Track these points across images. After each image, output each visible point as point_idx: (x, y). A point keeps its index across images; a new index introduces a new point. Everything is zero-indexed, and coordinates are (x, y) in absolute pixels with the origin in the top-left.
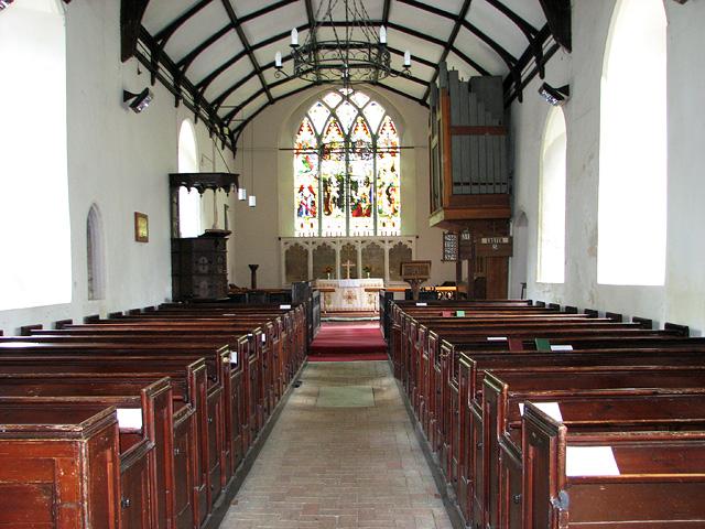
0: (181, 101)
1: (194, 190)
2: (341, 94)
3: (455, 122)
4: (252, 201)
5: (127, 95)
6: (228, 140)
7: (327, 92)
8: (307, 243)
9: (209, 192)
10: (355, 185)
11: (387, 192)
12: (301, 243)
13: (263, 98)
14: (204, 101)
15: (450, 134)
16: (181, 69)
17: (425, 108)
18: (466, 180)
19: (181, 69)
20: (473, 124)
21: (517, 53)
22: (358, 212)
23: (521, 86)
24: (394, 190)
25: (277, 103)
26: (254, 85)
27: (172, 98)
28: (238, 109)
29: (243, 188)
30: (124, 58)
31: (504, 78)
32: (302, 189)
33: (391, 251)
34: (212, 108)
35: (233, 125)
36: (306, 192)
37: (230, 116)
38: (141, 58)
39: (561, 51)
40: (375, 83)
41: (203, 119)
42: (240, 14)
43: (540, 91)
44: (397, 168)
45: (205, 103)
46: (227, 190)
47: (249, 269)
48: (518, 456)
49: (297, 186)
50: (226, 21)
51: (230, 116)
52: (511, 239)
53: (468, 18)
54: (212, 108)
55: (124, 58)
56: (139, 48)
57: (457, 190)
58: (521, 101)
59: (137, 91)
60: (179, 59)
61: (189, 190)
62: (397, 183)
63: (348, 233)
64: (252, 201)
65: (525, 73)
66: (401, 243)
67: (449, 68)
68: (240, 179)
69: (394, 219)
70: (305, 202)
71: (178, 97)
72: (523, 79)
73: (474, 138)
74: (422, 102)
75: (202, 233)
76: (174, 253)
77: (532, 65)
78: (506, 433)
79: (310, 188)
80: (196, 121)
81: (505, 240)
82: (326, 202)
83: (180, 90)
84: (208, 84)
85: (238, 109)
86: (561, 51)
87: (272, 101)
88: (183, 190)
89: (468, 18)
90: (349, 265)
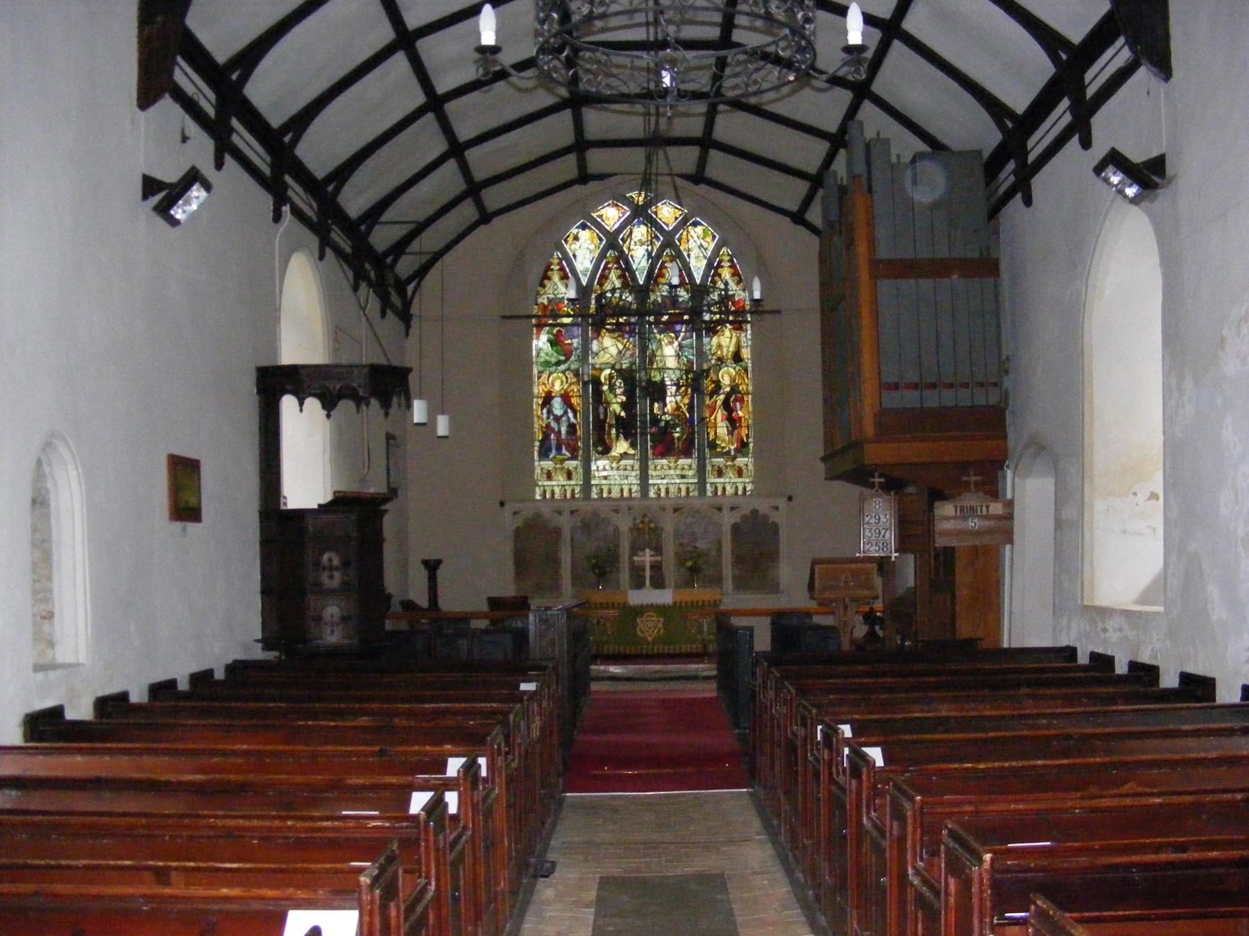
0: (286, 209)
1: (313, 404)
2: (629, 202)
3: (883, 253)
4: (443, 426)
5: (150, 186)
6: (395, 299)
7: (599, 201)
8: (560, 513)
9: (345, 406)
10: (658, 392)
11: (726, 405)
12: (545, 510)
13: (467, 211)
14: (370, 249)
15: (874, 277)
16: (287, 139)
17: (802, 231)
18: (912, 376)
19: (287, 139)
20: (924, 254)
21: (1019, 100)
22: (664, 445)
23: (1026, 173)
24: (742, 401)
25: (497, 222)
26: (448, 179)
27: (268, 201)
28: (420, 228)
29: (420, 398)
30: (146, 99)
31: (986, 154)
32: (548, 399)
33: (736, 529)
34: (359, 228)
35: (405, 266)
36: (557, 405)
37: (399, 248)
38: (190, 106)
39: (1143, 73)
40: (698, 177)
41: (339, 252)
42: (413, 20)
43: (1099, 169)
44: (746, 353)
45: (339, 215)
46: (386, 405)
47: (422, 568)
48: (937, 893)
49: (539, 390)
50: (420, 99)
51: (399, 248)
52: (1010, 504)
53: (909, 25)
54: (359, 228)
55: (146, 99)
56: (179, 77)
57: (892, 400)
58: (1028, 201)
59: (171, 175)
60: (285, 118)
61: (301, 404)
62: (747, 385)
63: (665, 153)
64: (443, 426)
65: (1038, 142)
66: (755, 512)
67: (870, 134)
68: (413, 380)
69: (741, 461)
70: (554, 425)
71: (280, 197)
72: (1031, 158)
73: (926, 284)
74: (798, 218)
75: (329, 498)
76: (267, 543)
77: (1060, 117)
78: (873, 814)
79: (566, 398)
80: (322, 257)
81: (996, 508)
82: (600, 425)
83: (286, 187)
84: (426, 273)
85: (420, 228)
86: (1143, 73)
87: (485, 217)
88: (288, 403)
89: (909, 25)
90: (647, 557)
